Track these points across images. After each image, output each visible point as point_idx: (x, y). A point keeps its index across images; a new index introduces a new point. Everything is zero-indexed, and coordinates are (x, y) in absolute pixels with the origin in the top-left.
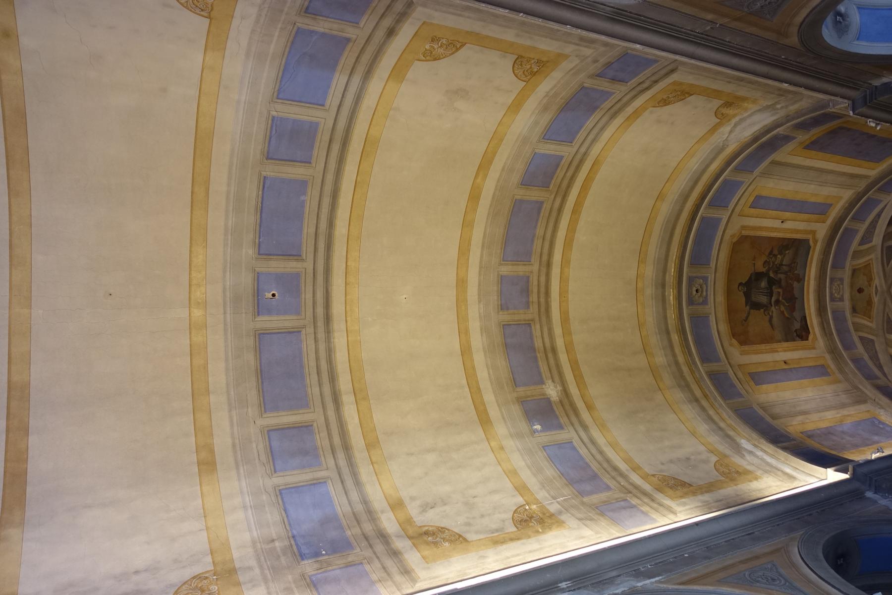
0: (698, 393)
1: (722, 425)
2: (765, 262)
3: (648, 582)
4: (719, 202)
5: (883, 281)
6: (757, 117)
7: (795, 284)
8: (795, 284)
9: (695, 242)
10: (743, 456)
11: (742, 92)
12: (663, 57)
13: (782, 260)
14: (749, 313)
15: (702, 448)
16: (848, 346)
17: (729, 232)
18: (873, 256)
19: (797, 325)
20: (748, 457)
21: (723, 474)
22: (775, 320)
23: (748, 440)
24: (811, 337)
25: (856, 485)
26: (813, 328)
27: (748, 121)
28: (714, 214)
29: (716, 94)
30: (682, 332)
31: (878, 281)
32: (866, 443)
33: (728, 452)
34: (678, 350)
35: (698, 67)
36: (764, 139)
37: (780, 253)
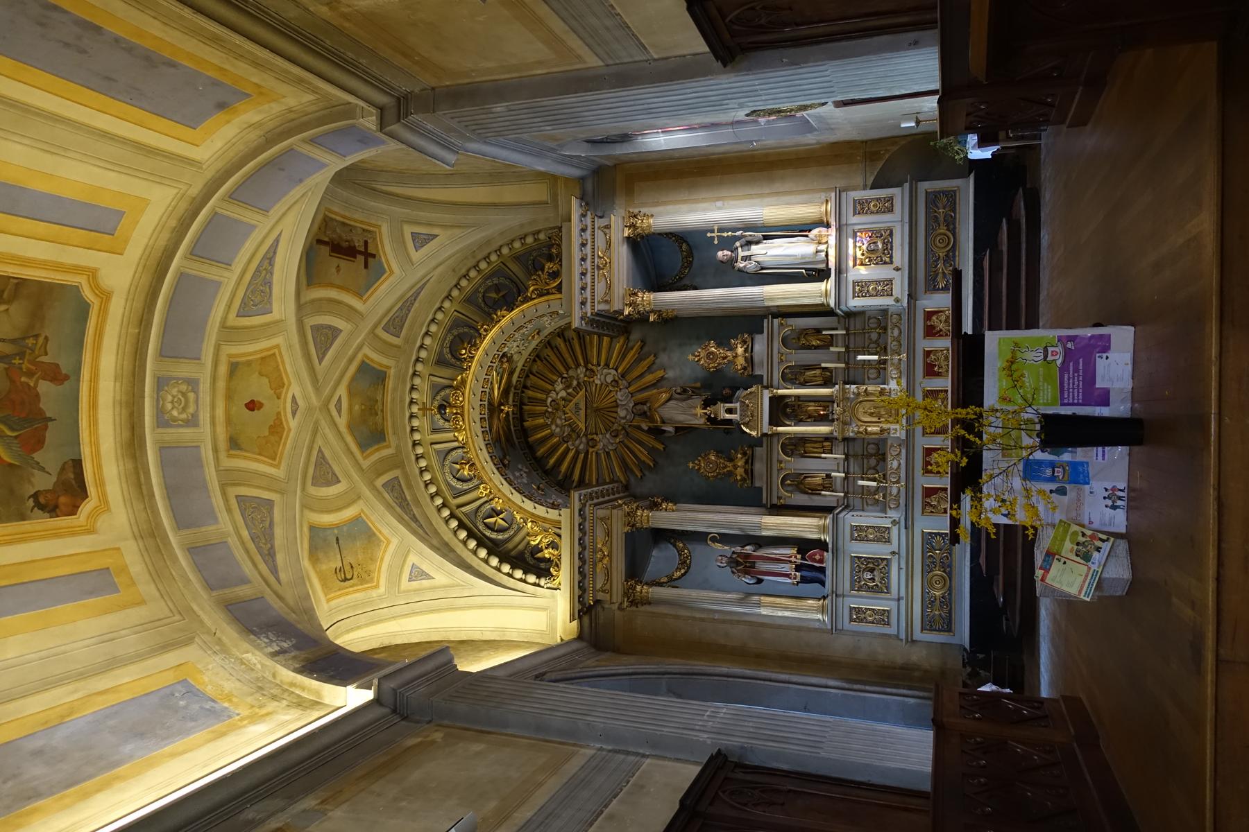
7: (45, 387)
26: (101, 483)
31: (298, 388)
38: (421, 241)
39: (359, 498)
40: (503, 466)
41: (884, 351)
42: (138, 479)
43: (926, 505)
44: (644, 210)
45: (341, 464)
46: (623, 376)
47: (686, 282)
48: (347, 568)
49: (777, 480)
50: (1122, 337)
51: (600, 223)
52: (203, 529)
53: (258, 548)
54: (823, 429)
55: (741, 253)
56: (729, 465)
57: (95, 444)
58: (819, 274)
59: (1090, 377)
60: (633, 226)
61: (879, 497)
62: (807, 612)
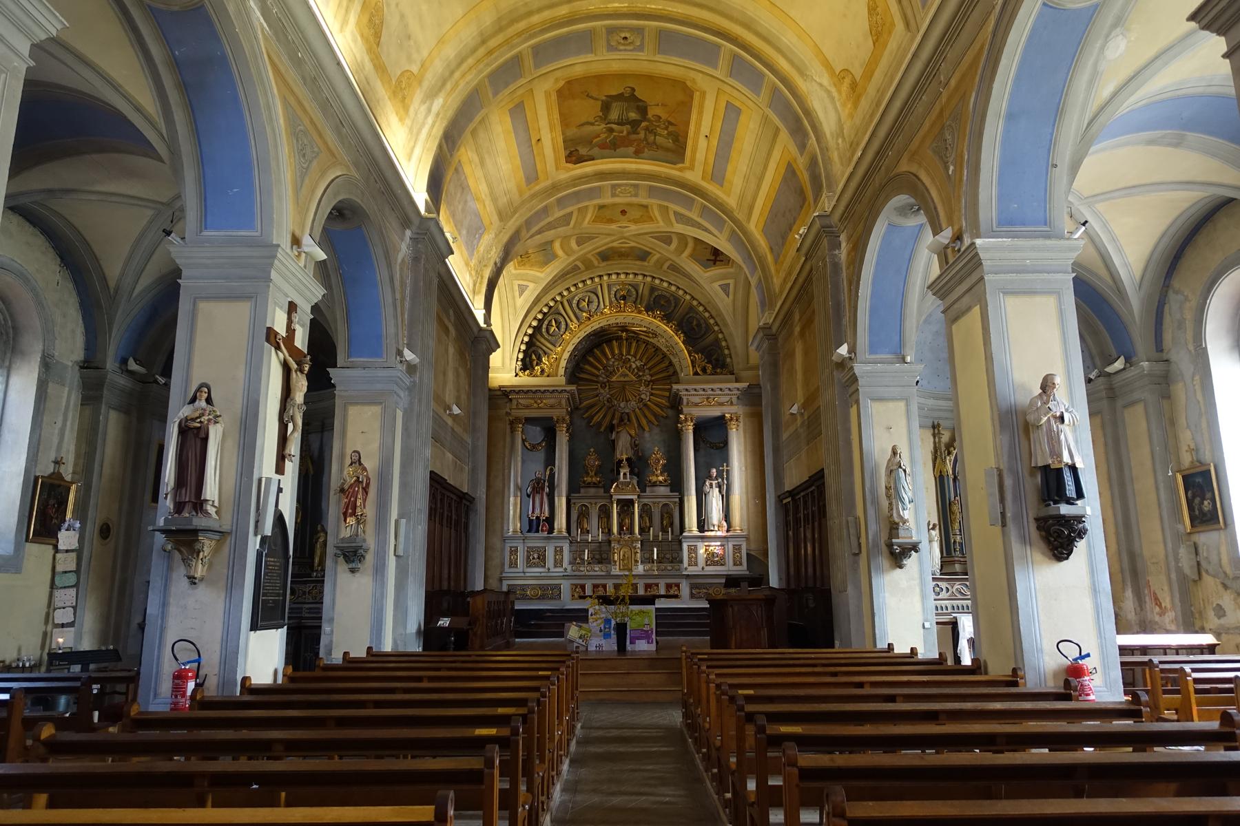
0: (493, 43)
1: (457, 75)
3: (259, 14)
4: (738, 68)
6: (832, 117)
7: (631, 150)
8: (631, 150)
10: (423, 102)
11: (865, 103)
12: (926, 14)
13: (660, 135)
15: (425, 53)
16: (560, 202)
17: (699, 78)
18: (661, 223)
19: (583, 151)
20: (423, 108)
21: (399, 82)
22: (591, 128)
23: (443, 106)
24: (570, 165)
25: (416, 221)
27: (830, 107)
28: (723, 62)
29: (869, 73)
30: (571, 20)
32: (458, 225)
33: (426, 84)
34: (547, 14)
35: (904, 56)
36: (806, 122)
37: (670, 134)
38: (725, 288)
40: (588, 336)
41: (660, 561)
43: (576, 586)
44: (741, 425)
45: (588, 247)
46: (645, 405)
47: (702, 445)
49: (585, 502)
50: (653, 647)
51: (734, 399)
54: (615, 529)
55: (714, 483)
56: (595, 474)
58: (702, 526)
59: (639, 638)
60: (731, 419)
61: (578, 561)
62: (513, 523)
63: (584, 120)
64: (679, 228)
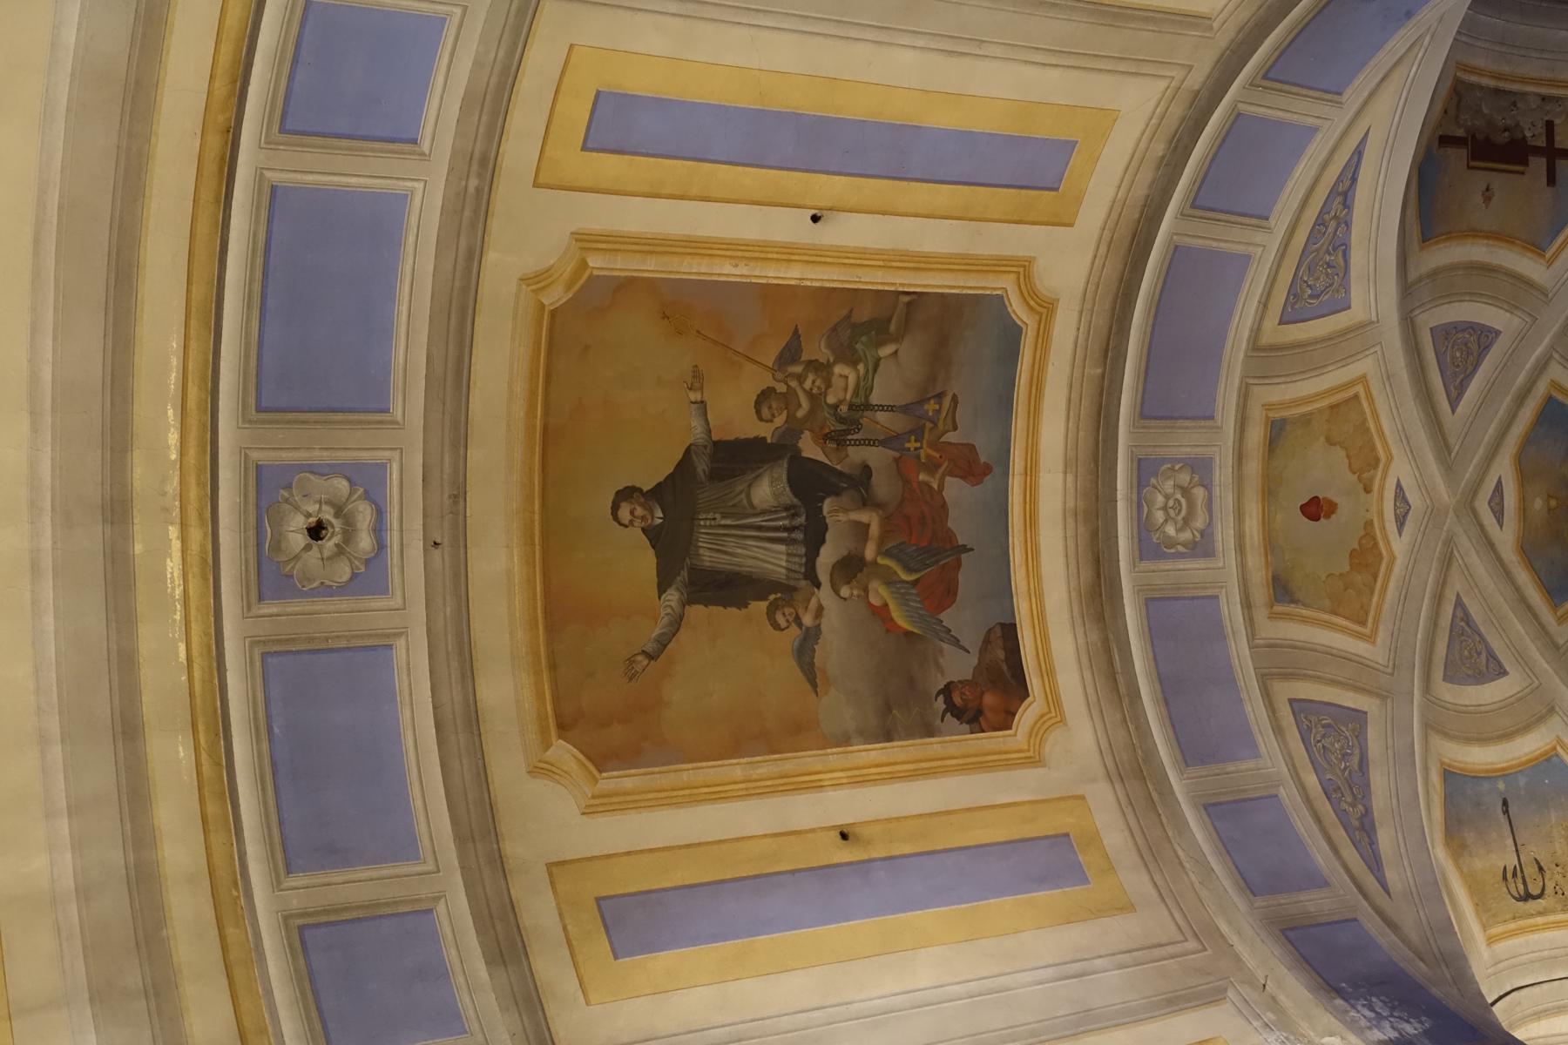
2: (765, 396)
5: (1434, 469)
7: (955, 490)
8: (955, 490)
9: (263, 303)
13: (864, 387)
14: (677, 623)
18: (1365, 365)
24: (1027, 716)
26: (1048, 673)
31: (1407, 467)
39: (1551, 710)
42: (1111, 663)
48: (1531, 871)
52: (1231, 767)
53: (1342, 816)
57: (1037, 594)
63: (788, 666)
64: (1372, 290)
